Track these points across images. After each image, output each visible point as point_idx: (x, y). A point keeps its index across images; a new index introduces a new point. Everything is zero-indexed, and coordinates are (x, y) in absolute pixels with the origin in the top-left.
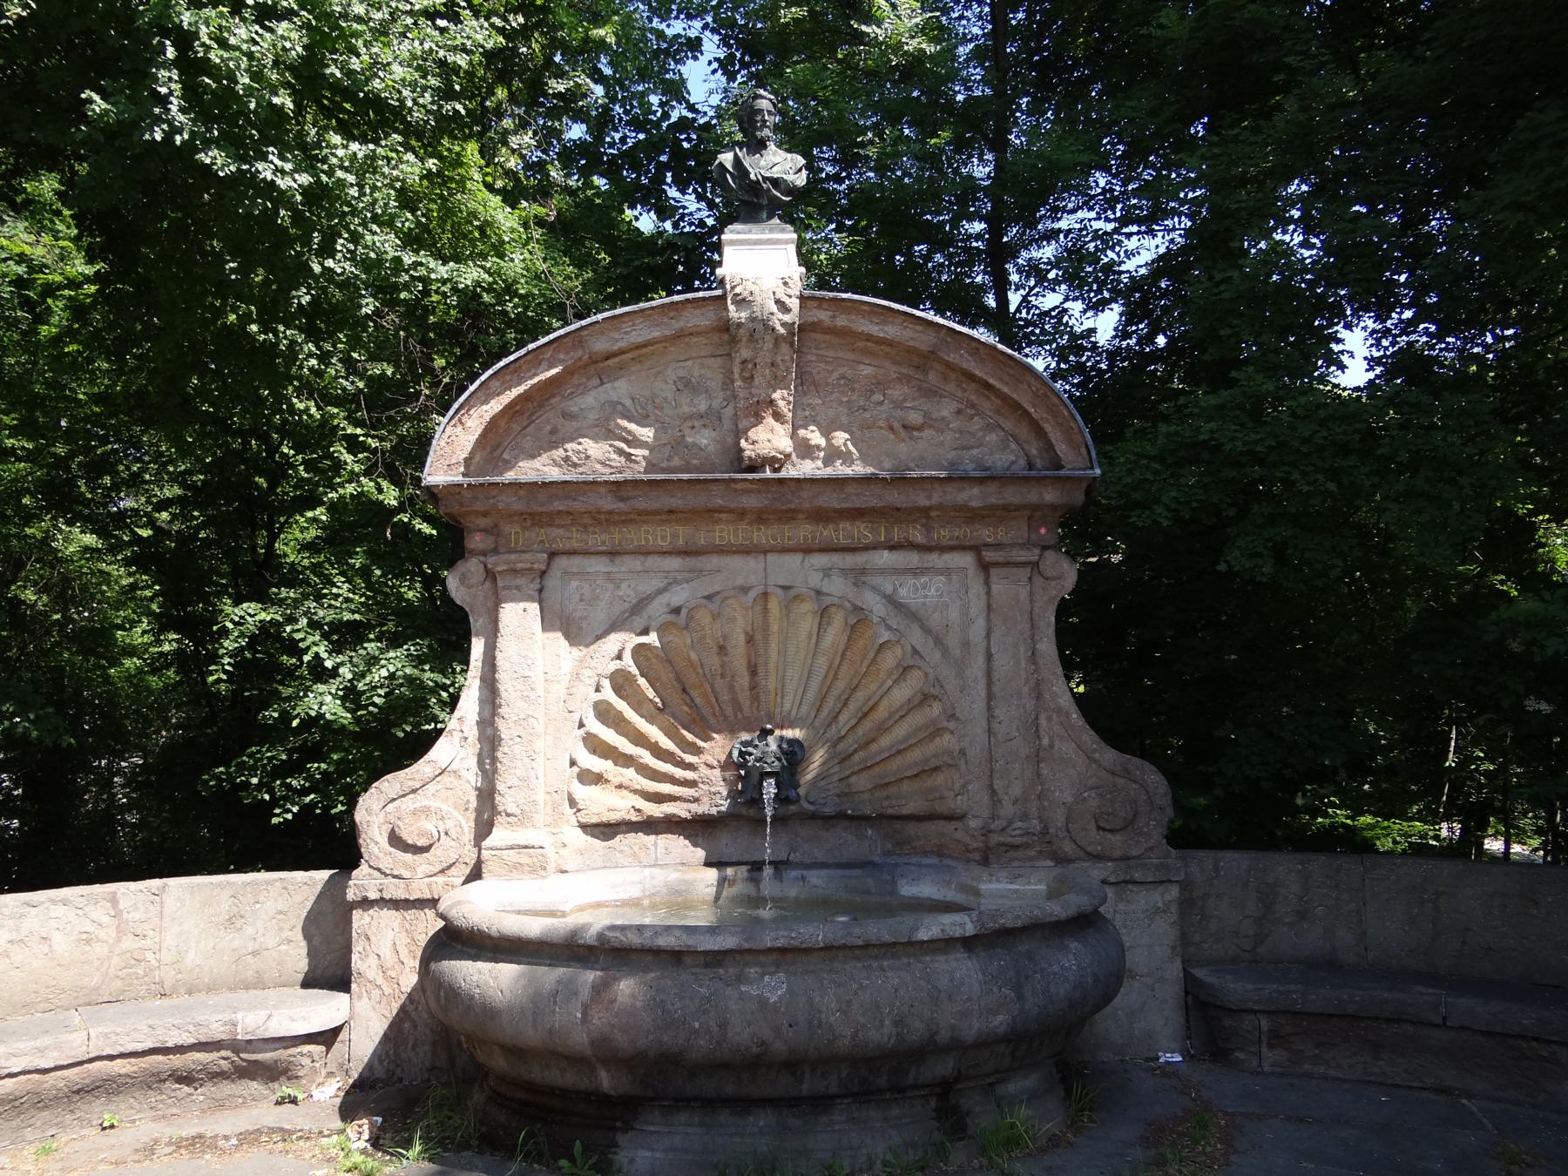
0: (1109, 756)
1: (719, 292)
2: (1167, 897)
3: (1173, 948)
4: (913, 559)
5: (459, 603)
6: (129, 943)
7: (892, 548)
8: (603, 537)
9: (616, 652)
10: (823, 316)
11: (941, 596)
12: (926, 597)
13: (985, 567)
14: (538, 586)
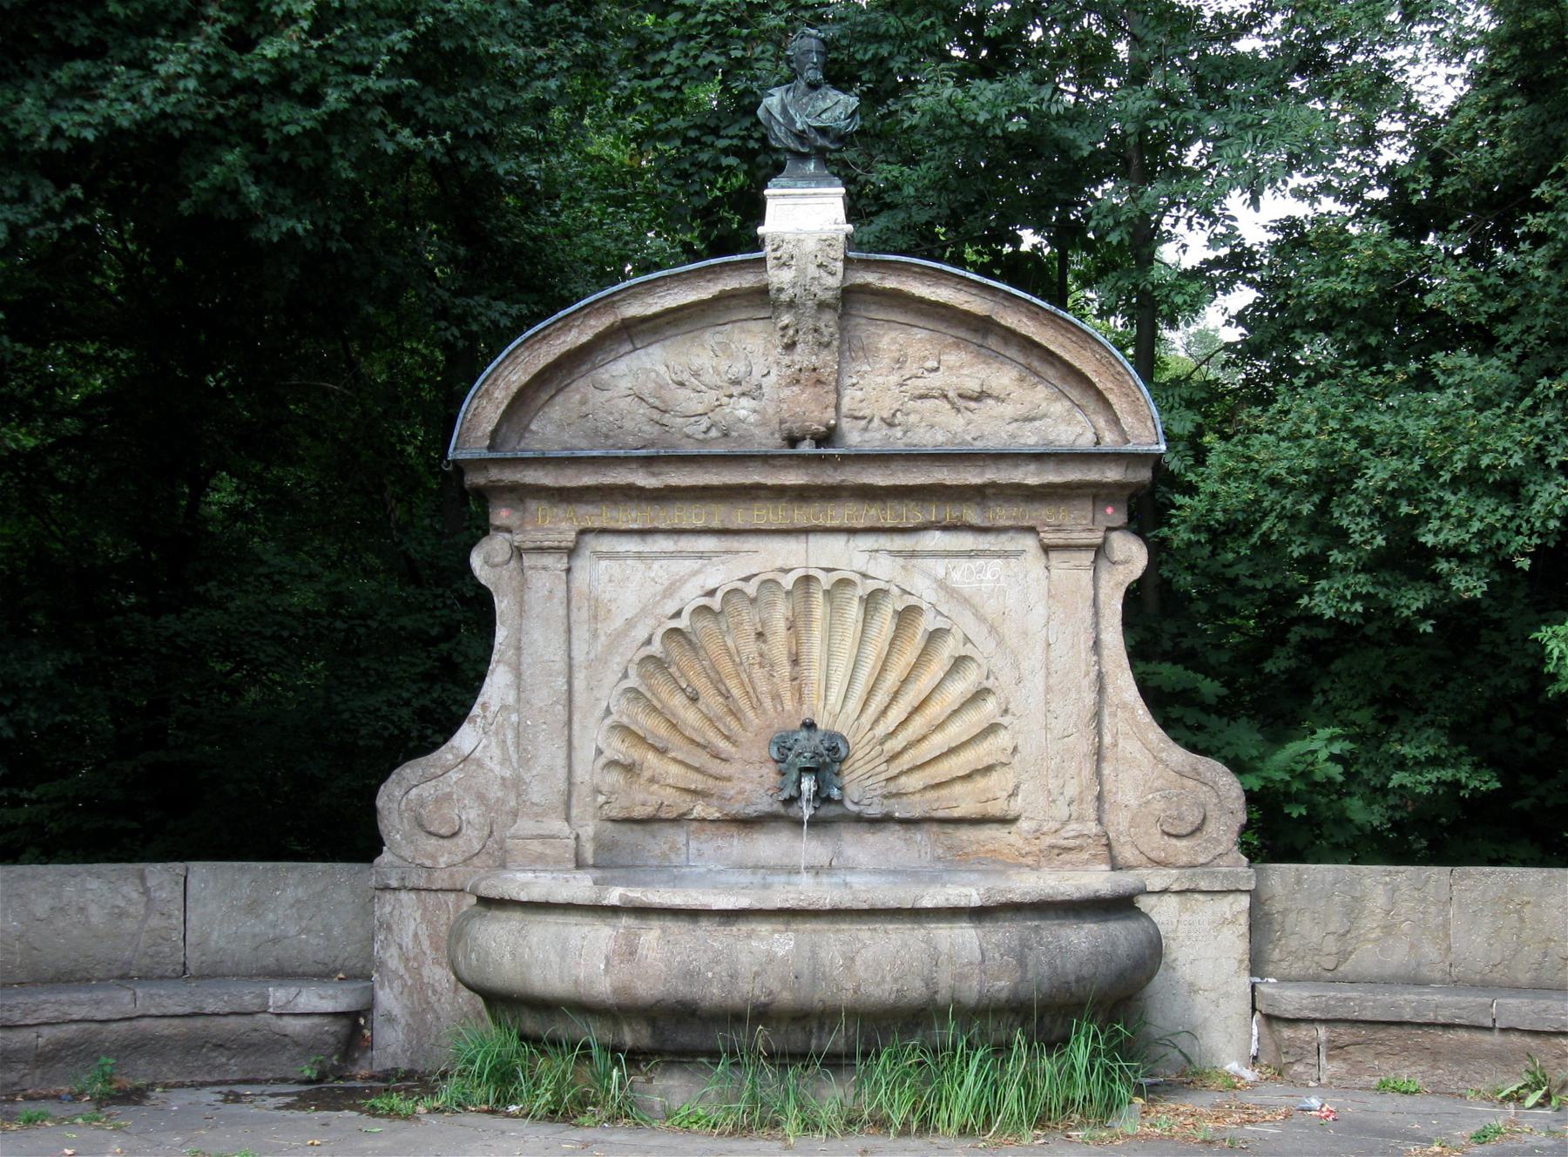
0: (1179, 755)
2: (1236, 908)
3: (1241, 961)
4: (967, 541)
6: (155, 921)
7: (946, 528)
14: (565, 566)
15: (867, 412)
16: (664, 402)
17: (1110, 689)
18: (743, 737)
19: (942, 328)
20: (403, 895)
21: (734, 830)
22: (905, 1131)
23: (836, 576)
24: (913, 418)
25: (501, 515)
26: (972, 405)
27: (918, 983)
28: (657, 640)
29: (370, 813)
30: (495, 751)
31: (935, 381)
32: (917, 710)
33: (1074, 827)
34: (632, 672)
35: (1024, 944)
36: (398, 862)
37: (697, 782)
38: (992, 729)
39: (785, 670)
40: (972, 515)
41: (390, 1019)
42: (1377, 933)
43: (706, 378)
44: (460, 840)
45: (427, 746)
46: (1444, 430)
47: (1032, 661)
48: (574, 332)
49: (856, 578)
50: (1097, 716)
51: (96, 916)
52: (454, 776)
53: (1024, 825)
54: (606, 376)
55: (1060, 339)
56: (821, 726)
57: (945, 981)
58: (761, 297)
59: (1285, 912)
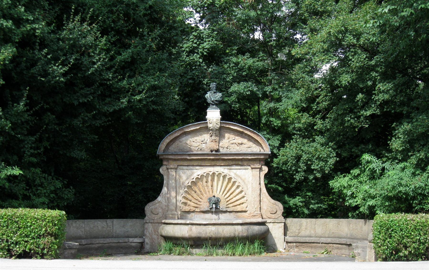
0: (273, 201)
2: (282, 225)
4: (239, 167)
6: (108, 229)
15: (223, 146)
17: (262, 190)
18: (203, 198)
20: (149, 224)
21: (202, 213)
22: (231, 255)
23: (218, 173)
24: (231, 147)
25: (165, 163)
26: (240, 145)
27: (233, 234)
28: (190, 183)
29: (143, 210)
30: (164, 201)
31: (234, 141)
32: (231, 194)
33: (256, 212)
35: (248, 229)
36: (148, 218)
37: (196, 205)
38: (243, 197)
39: (210, 187)
40: (240, 163)
41: (147, 243)
42: (304, 229)
43: (197, 141)
44: (159, 215)
46: (315, 150)
47: (250, 186)
48: (177, 134)
49: (222, 173)
50: (260, 195)
51: (100, 228)
52: (157, 205)
53: (248, 212)
56: (216, 196)
57: (237, 234)
58: (207, 129)
59: (290, 226)
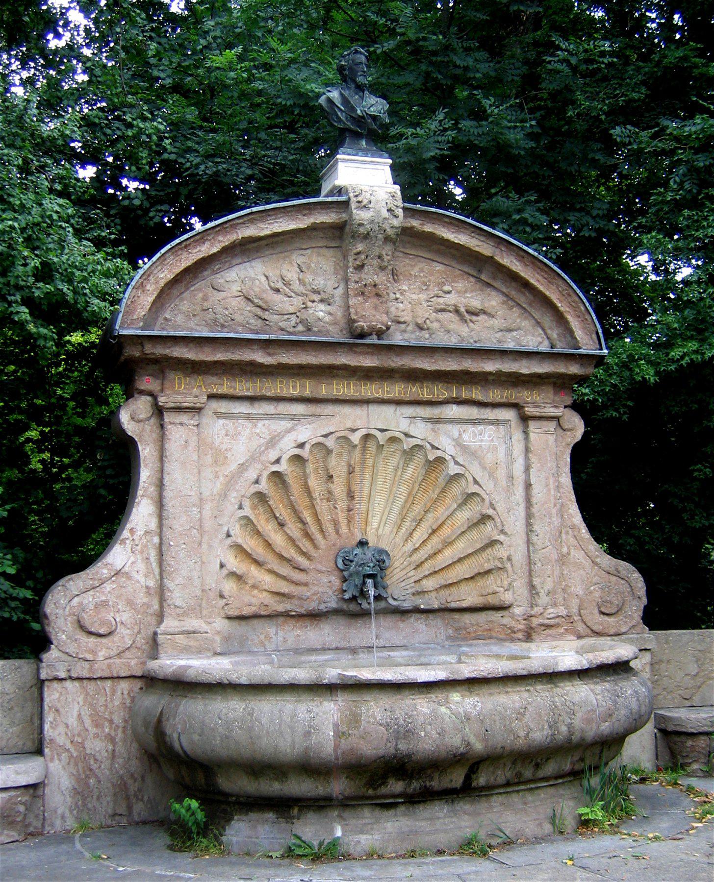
0: (607, 561)
1: (343, 198)
2: (644, 661)
4: (473, 412)
5: (130, 433)
8: (247, 385)
9: (256, 477)
10: (415, 223)
11: (492, 440)
12: (482, 441)
13: (525, 419)
16: (266, 302)
19: (453, 263)
20: (68, 684)
23: (388, 434)
30: (141, 566)
34: (247, 504)
39: (342, 505)
44: (116, 638)
45: (84, 563)
48: (207, 244)
52: (108, 587)
54: (222, 281)
55: (537, 275)
